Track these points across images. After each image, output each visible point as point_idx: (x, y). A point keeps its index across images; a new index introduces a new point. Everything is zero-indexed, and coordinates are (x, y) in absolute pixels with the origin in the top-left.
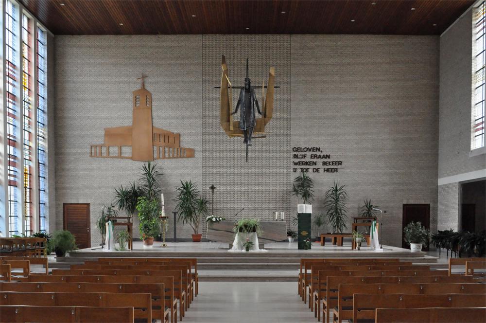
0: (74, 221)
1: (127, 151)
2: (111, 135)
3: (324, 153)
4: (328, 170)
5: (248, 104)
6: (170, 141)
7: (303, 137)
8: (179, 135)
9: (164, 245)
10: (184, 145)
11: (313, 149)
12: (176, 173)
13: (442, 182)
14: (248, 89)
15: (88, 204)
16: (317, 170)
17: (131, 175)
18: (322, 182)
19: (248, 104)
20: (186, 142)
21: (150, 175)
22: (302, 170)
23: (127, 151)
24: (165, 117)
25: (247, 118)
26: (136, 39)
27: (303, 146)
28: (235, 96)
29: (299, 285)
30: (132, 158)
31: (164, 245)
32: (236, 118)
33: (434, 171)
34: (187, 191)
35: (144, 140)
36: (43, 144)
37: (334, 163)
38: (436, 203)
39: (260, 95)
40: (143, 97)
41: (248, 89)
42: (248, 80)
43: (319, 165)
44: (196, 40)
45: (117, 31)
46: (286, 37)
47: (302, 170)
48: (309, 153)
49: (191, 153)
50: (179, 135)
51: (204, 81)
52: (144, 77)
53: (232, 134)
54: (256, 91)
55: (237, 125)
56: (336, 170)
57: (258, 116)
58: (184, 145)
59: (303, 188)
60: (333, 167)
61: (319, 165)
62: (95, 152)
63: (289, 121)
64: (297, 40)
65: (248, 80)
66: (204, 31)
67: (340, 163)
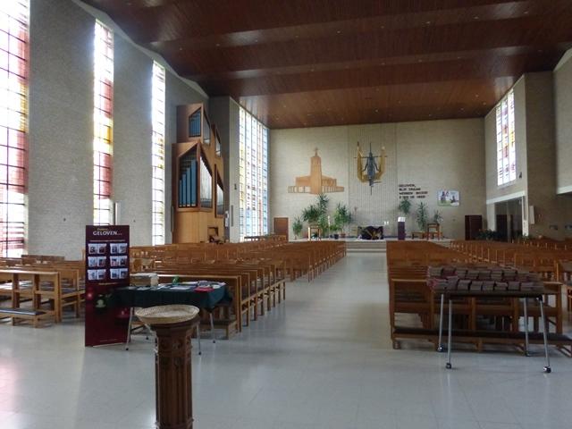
0: (279, 226)
1: (308, 189)
2: (300, 181)
3: (417, 187)
4: (419, 197)
5: (371, 166)
6: (331, 182)
7: (403, 179)
8: (335, 180)
9: (449, 366)
10: (338, 185)
11: (410, 185)
12: (337, 200)
13: (488, 202)
14: (371, 158)
15: (287, 219)
16: (413, 197)
17: (311, 201)
18: (416, 202)
19: (371, 166)
20: (339, 184)
21: (323, 202)
22: (404, 197)
23: (308, 189)
24: (328, 170)
25: (371, 173)
26: (312, 129)
27: (405, 184)
28: (364, 162)
29: (229, 238)
30: (311, 193)
31: (449, 366)
32: (365, 173)
33: (484, 196)
34: (343, 212)
35: (316, 183)
36: (266, 187)
37: (423, 193)
38: (485, 213)
39: (377, 161)
40: (316, 160)
41: (371, 158)
42: (371, 154)
43: (414, 194)
44: (345, 128)
45: (303, 126)
46: (393, 124)
47: (404, 197)
48: (408, 188)
49: (342, 189)
50: (335, 180)
51: (349, 162)
52: (316, 149)
53: (363, 181)
54: (376, 159)
55: (366, 176)
56: (424, 197)
57: (376, 172)
58: (338, 185)
59: (405, 207)
60: (422, 195)
61: (414, 194)
62: (291, 190)
63: (396, 170)
64: (399, 124)
65: (371, 154)
66: (348, 124)
67: (426, 193)
